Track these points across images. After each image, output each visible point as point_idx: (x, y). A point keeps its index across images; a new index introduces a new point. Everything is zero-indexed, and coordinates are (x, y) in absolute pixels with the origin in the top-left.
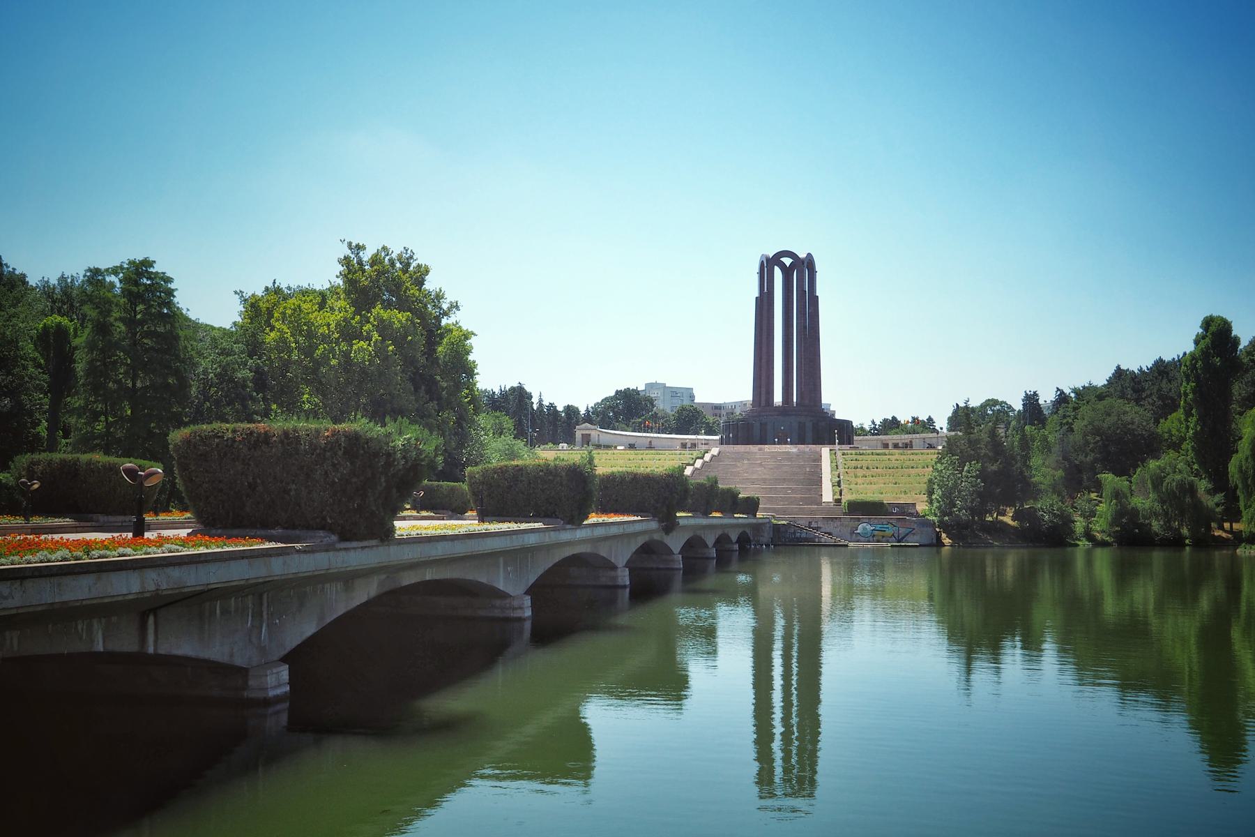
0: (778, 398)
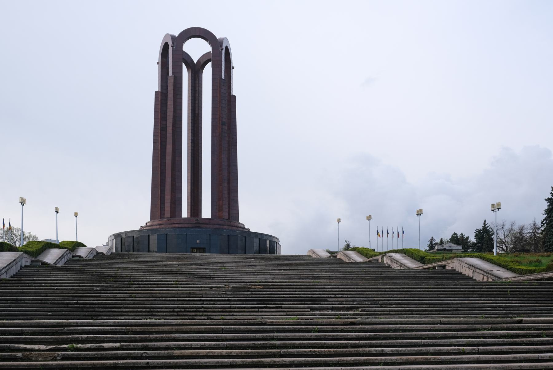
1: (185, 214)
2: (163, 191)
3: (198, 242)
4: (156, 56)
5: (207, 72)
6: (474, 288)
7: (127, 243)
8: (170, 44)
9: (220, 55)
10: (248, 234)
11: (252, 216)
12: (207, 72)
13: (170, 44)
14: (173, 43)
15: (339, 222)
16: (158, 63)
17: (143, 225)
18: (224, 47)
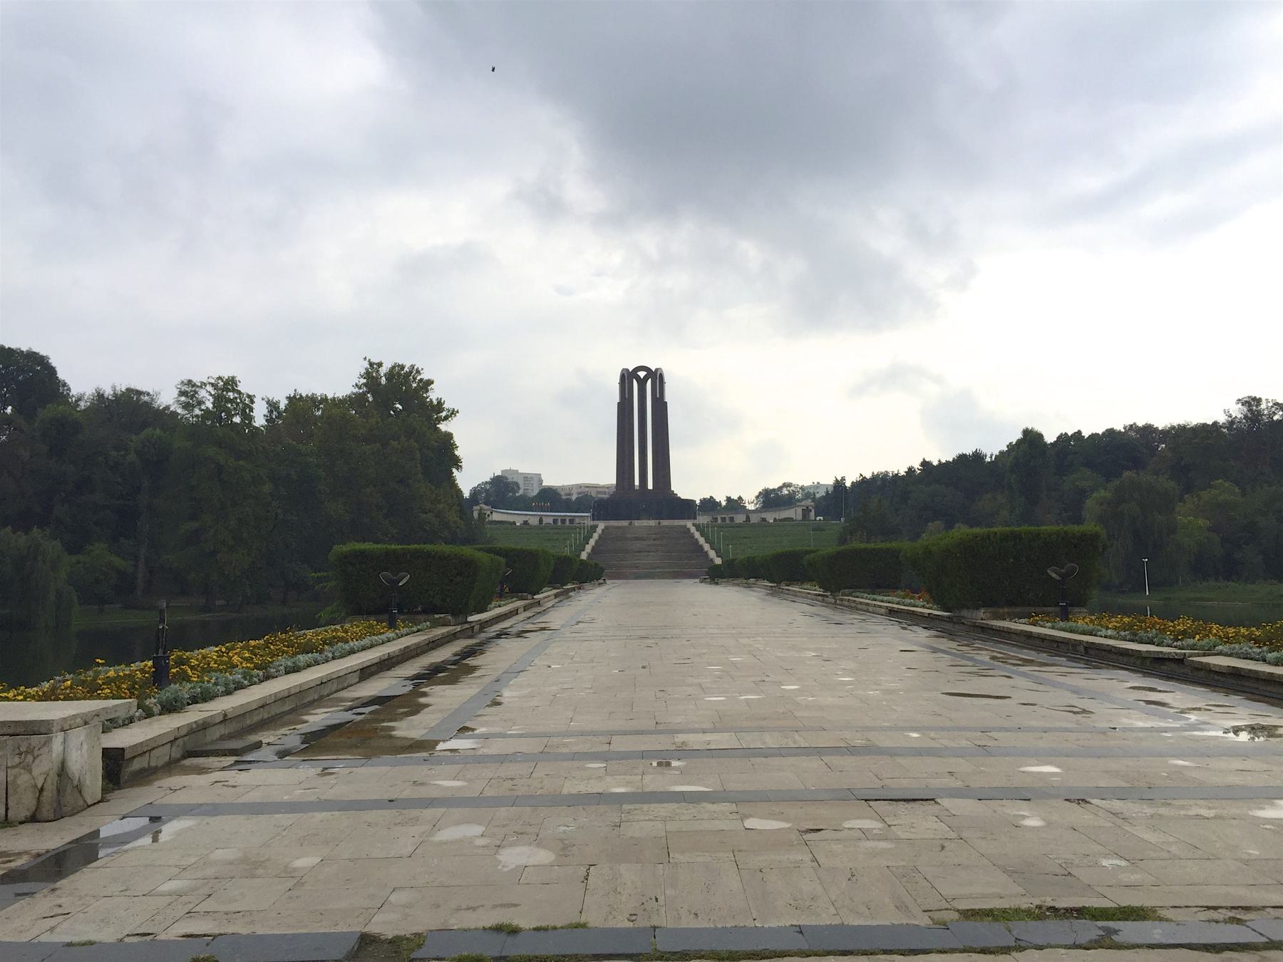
9: (657, 377)
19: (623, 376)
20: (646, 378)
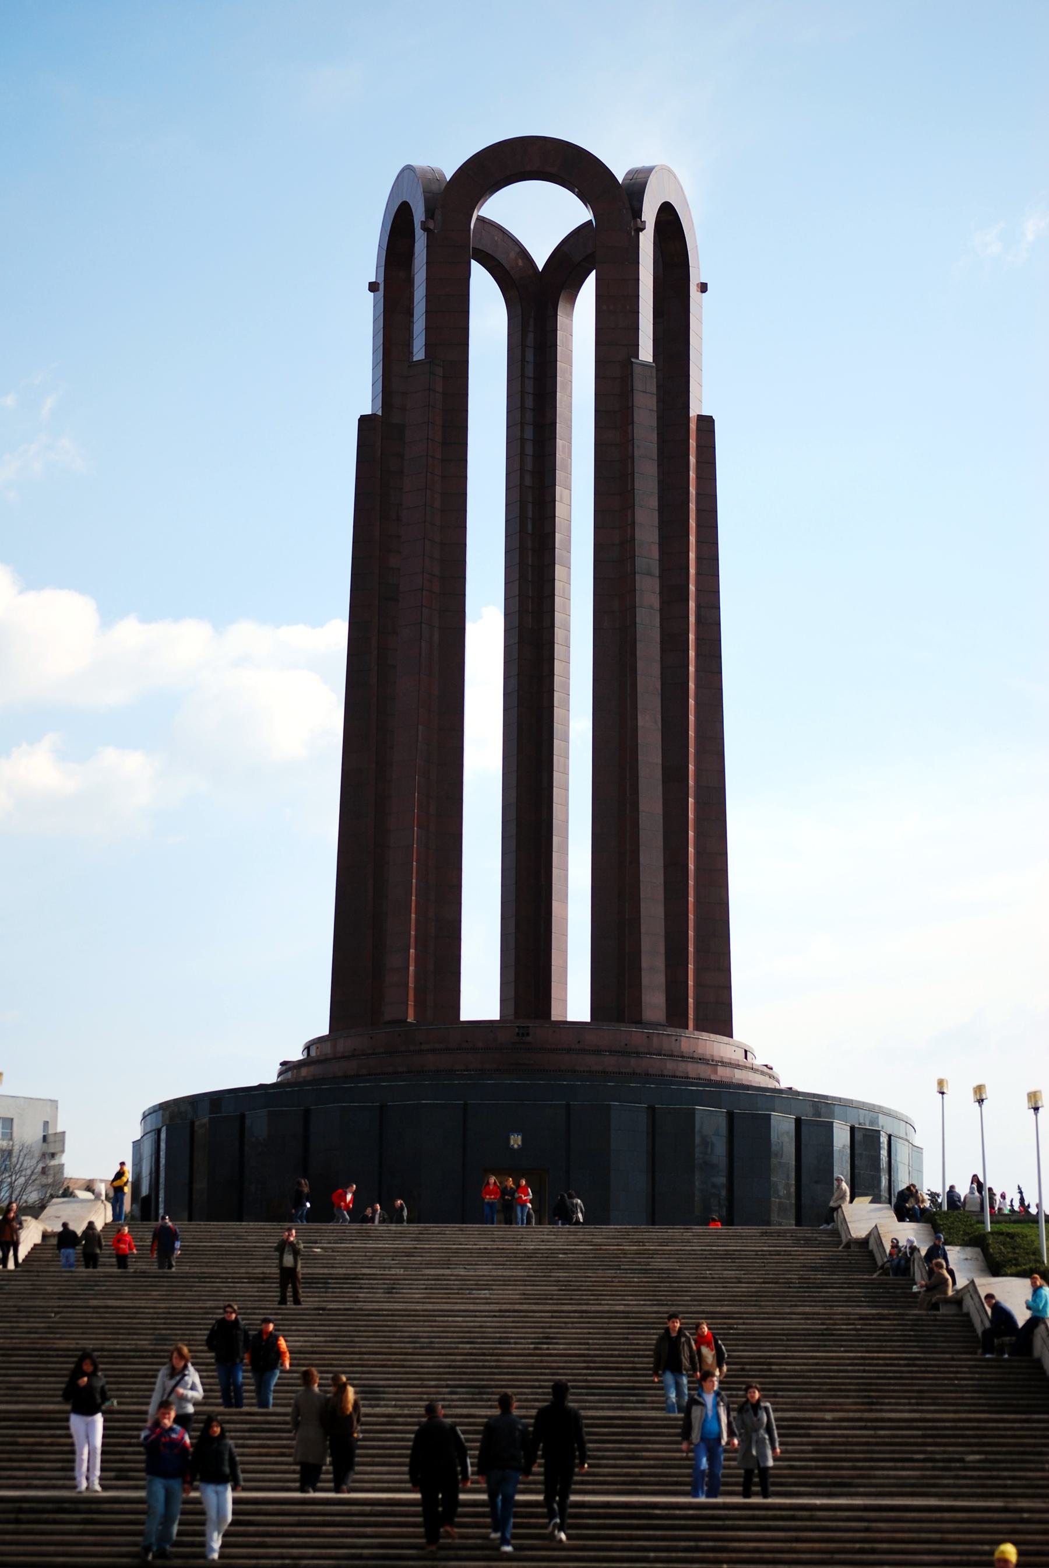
0: (481, 996)
1: (481, 996)
2: (673, 643)
3: (516, 1141)
4: (367, 264)
5: (580, 322)
6: (770, 1370)
7: (208, 1146)
8: (419, 215)
9: (632, 246)
10: (751, 1108)
11: (804, 1009)
12: (580, 322)
13: (419, 215)
14: (430, 213)
15: (981, 1101)
16: (373, 287)
17: (296, 1055)
18: (649, 214)
19: (399, 227)
20: (573, 258)
